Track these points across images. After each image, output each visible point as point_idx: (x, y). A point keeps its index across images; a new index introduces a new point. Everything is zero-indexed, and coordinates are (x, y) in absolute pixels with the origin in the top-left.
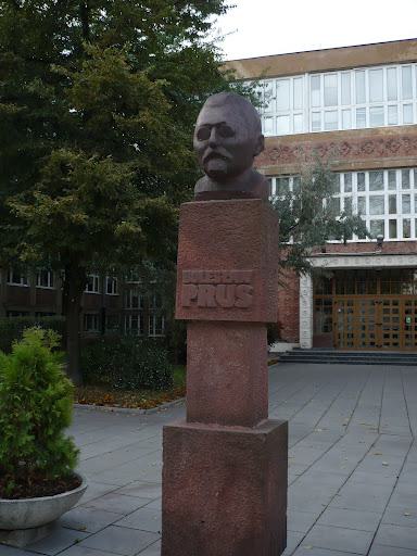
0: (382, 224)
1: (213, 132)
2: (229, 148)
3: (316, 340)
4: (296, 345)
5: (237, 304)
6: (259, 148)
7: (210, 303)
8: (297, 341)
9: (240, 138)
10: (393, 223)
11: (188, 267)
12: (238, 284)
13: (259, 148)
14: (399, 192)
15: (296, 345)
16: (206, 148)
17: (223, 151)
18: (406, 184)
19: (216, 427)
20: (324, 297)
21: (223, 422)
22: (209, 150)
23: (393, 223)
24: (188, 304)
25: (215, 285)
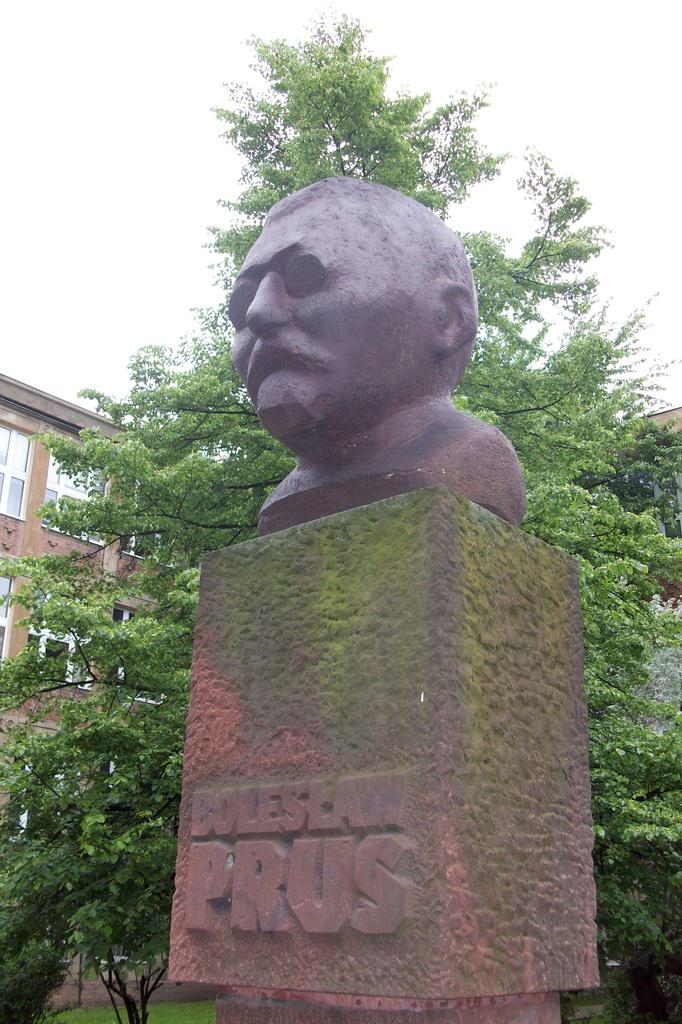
12: (361, 833)
17: (296, 341)
25: (288, 838)
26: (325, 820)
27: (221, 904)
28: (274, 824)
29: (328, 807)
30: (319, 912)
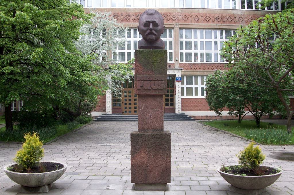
0: (190, 54)
1: (151, 24)
2: (156, 31)
3: (114, 110)
4: (104, 113)
5: (159, 88)
6: (163, 31)
7: (149, 87)
8: (105, 110)
9: (159, 28)
10: (196, 55)
11: (139, 74)
12: (159, 81)
13: (163, 31)
14: (199, 40)
15: (104, 113)
16: (147, 30)
17: (154, 32)
18: (202, 37)
19: (151, 133)
20: (172, 88)
21: (153, 130)
22: (148, 31)
23: (196, 55)
24: (140, 88)
25: (150, 81)
26: (155, 79)
27: (142, 87)
28: (149, 79)
29: (155, 78)
30: (154, 87)
